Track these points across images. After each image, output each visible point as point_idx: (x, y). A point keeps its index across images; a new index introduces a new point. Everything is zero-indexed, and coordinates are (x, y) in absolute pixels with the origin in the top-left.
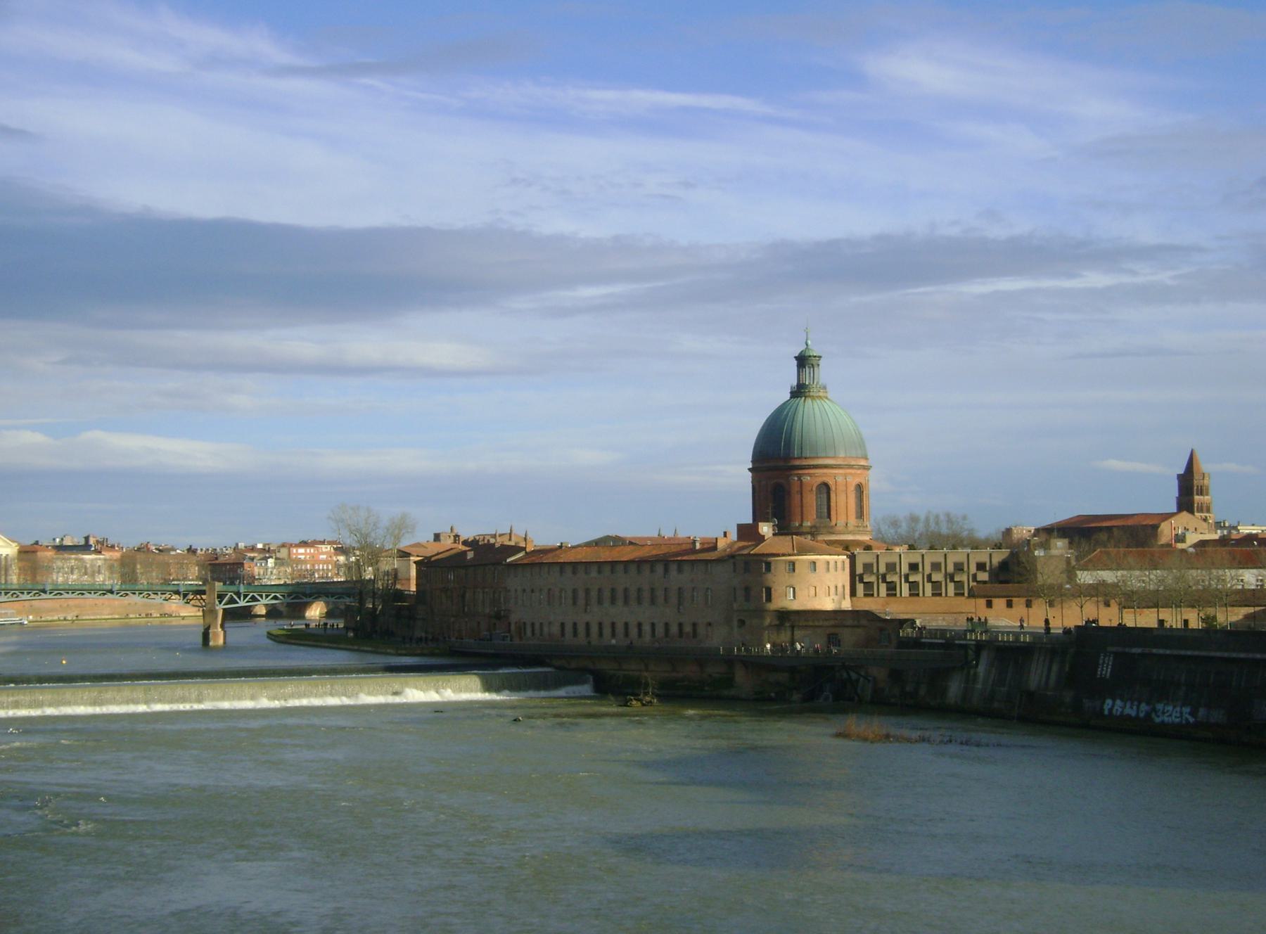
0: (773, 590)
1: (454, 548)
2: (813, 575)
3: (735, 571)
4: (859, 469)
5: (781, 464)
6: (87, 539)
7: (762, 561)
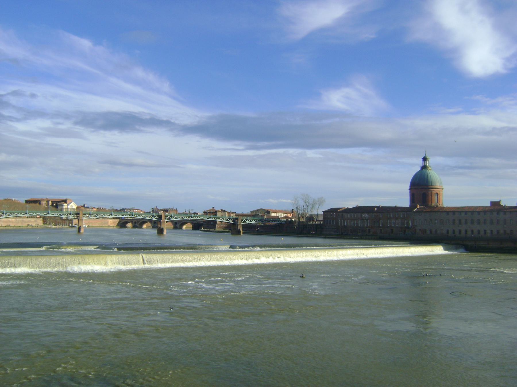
1: (343, 208)
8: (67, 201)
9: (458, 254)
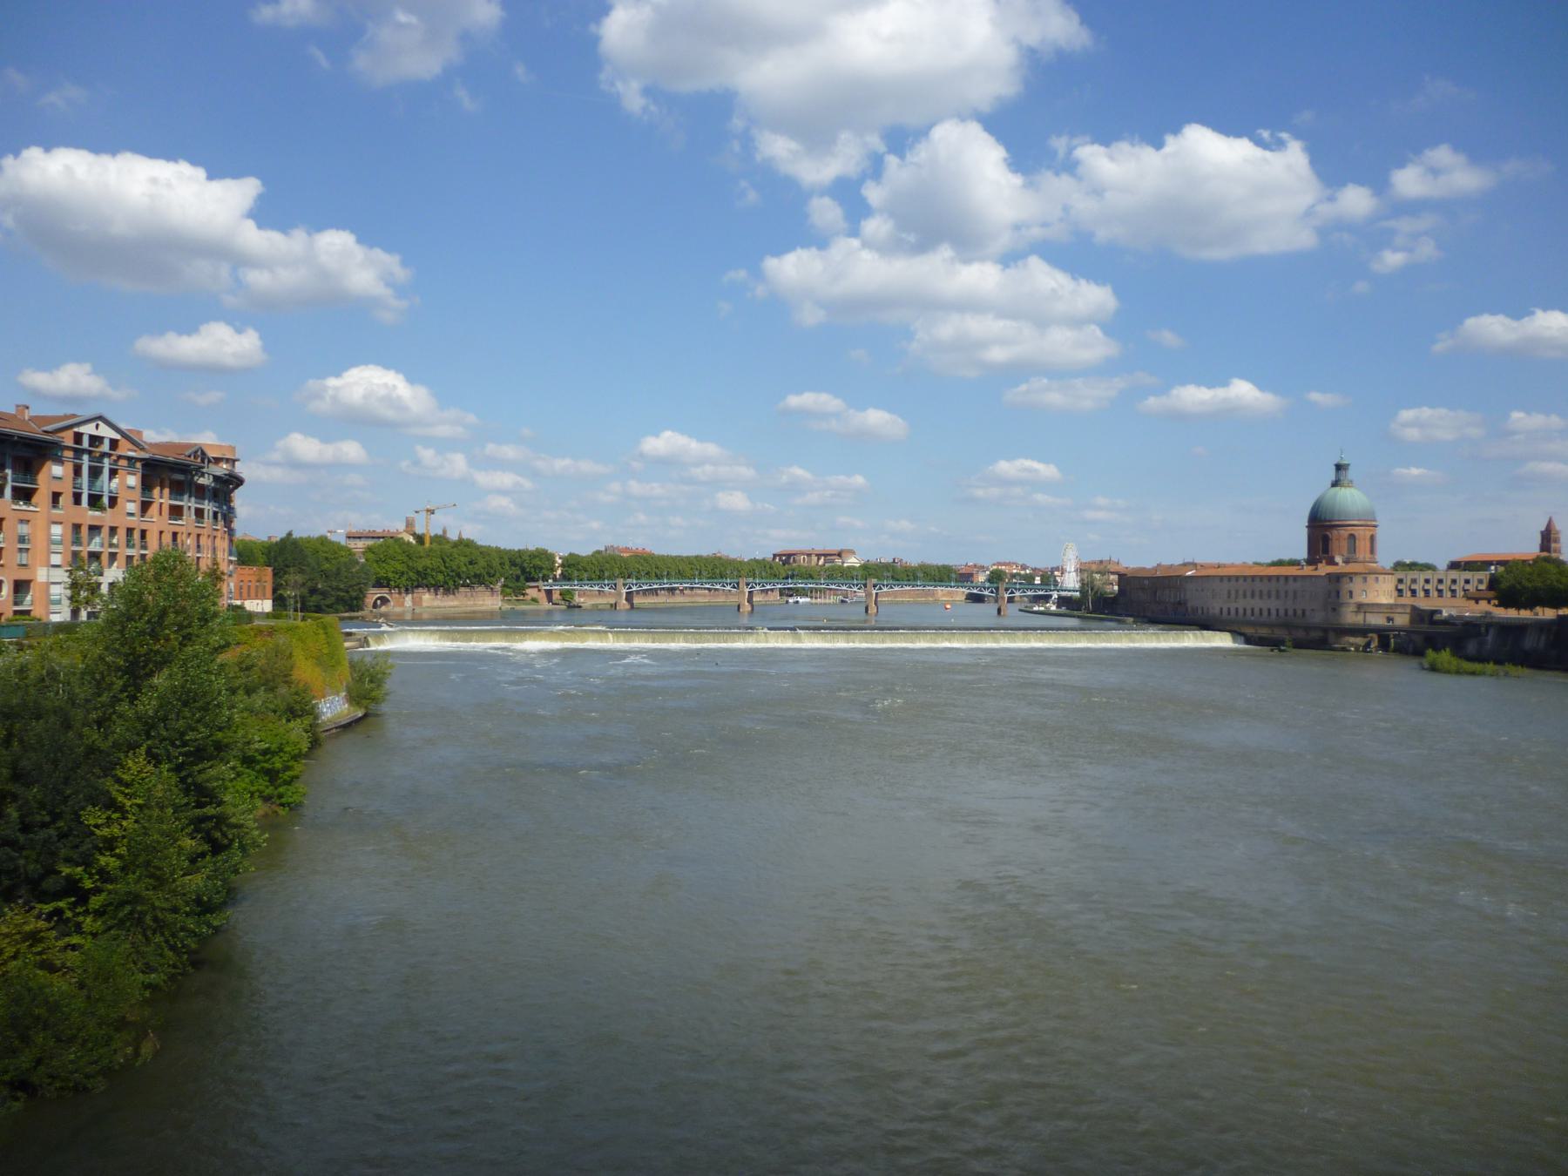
2: (1376, 585)
3: (1330, 581)
6: (894, 560)
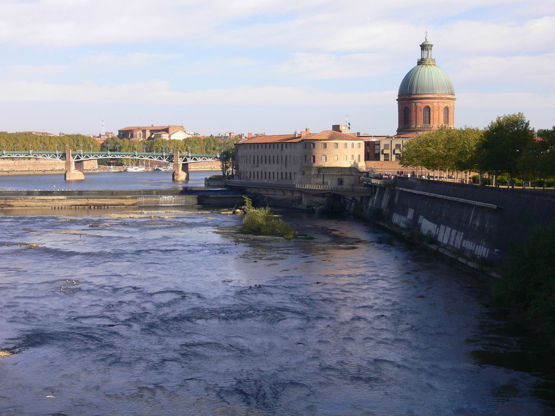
0: (316, 157)
4: (447, 99)
5: (407, 97)
7: (311, 143)
8: (170, 129)
9: (474, 212)
